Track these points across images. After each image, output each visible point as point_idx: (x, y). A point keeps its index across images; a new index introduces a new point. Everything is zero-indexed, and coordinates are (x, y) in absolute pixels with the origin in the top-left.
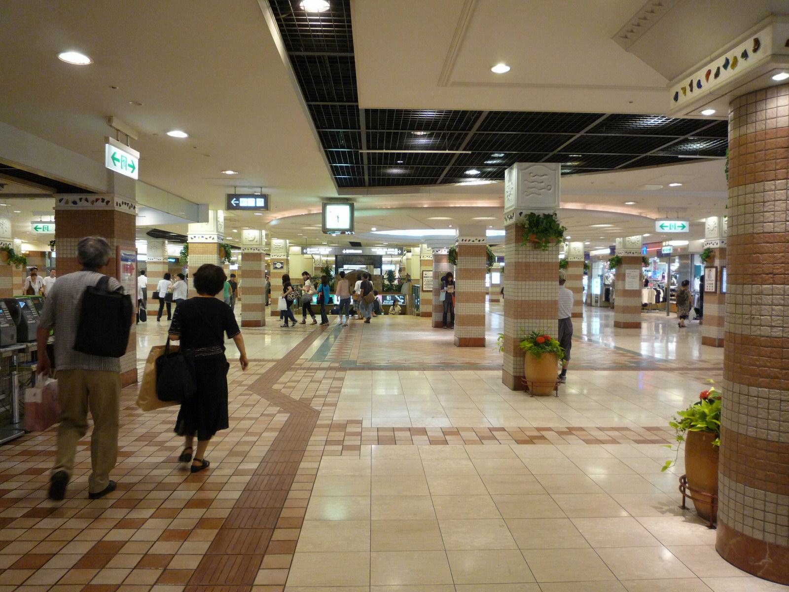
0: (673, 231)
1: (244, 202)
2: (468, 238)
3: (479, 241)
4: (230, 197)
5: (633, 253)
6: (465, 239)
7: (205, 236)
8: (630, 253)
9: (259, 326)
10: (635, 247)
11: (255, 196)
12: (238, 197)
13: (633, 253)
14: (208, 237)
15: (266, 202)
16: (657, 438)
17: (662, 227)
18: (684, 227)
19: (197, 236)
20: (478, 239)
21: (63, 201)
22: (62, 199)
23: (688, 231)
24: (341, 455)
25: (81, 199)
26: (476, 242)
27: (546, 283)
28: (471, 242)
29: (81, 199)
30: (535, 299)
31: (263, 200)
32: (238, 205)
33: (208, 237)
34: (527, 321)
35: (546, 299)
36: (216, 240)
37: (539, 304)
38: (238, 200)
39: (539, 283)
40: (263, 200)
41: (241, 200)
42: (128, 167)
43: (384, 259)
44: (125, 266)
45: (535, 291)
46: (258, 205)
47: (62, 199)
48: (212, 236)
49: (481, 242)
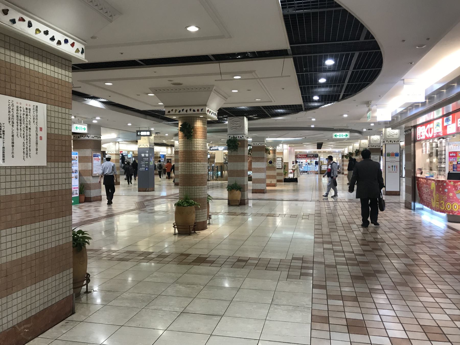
0: (341, 137)
1: (142, 133)
2: (256, 143)
3: (261, 144)
4: (138, 131)
5: (375, 146)
6: (254, 143)
7: (144, 145)
8: (374, 146)
9: (264, 193)
10: (376, 143)
11: (147, 131)
12: (140, 131)
13: (375, 146)
14: (145, 145)
15: (150, 133)
16: (450, 254)
17: (335, 136)
18: (347, 135)
19: (141, 145)
20: (261, 143)
21: (75, 137)
22: (187, 110)
23: (333, 138)
24: (277, 270)
25: (80, 136)
26: (260, 145)
27: (240, 163)
28: (257, 145)
29: (80, 136)
30: (236, 169)
31: (149, 132)
32: (140, 134)
33: (145, 145)
34: (233, 178)
35: (240, 169)
36: (149, 147)
37: (237, 171)
38: (140, 133)
39: (237, 163)
40: (149, 132)
41: (141, 132)
42: (79, 127)
43: (166, 156)
44: (95, 158)
45: (236, 166)
46: (147, 134)
47: (187, 110)
48: (147, 145)
49: (262, 145)
